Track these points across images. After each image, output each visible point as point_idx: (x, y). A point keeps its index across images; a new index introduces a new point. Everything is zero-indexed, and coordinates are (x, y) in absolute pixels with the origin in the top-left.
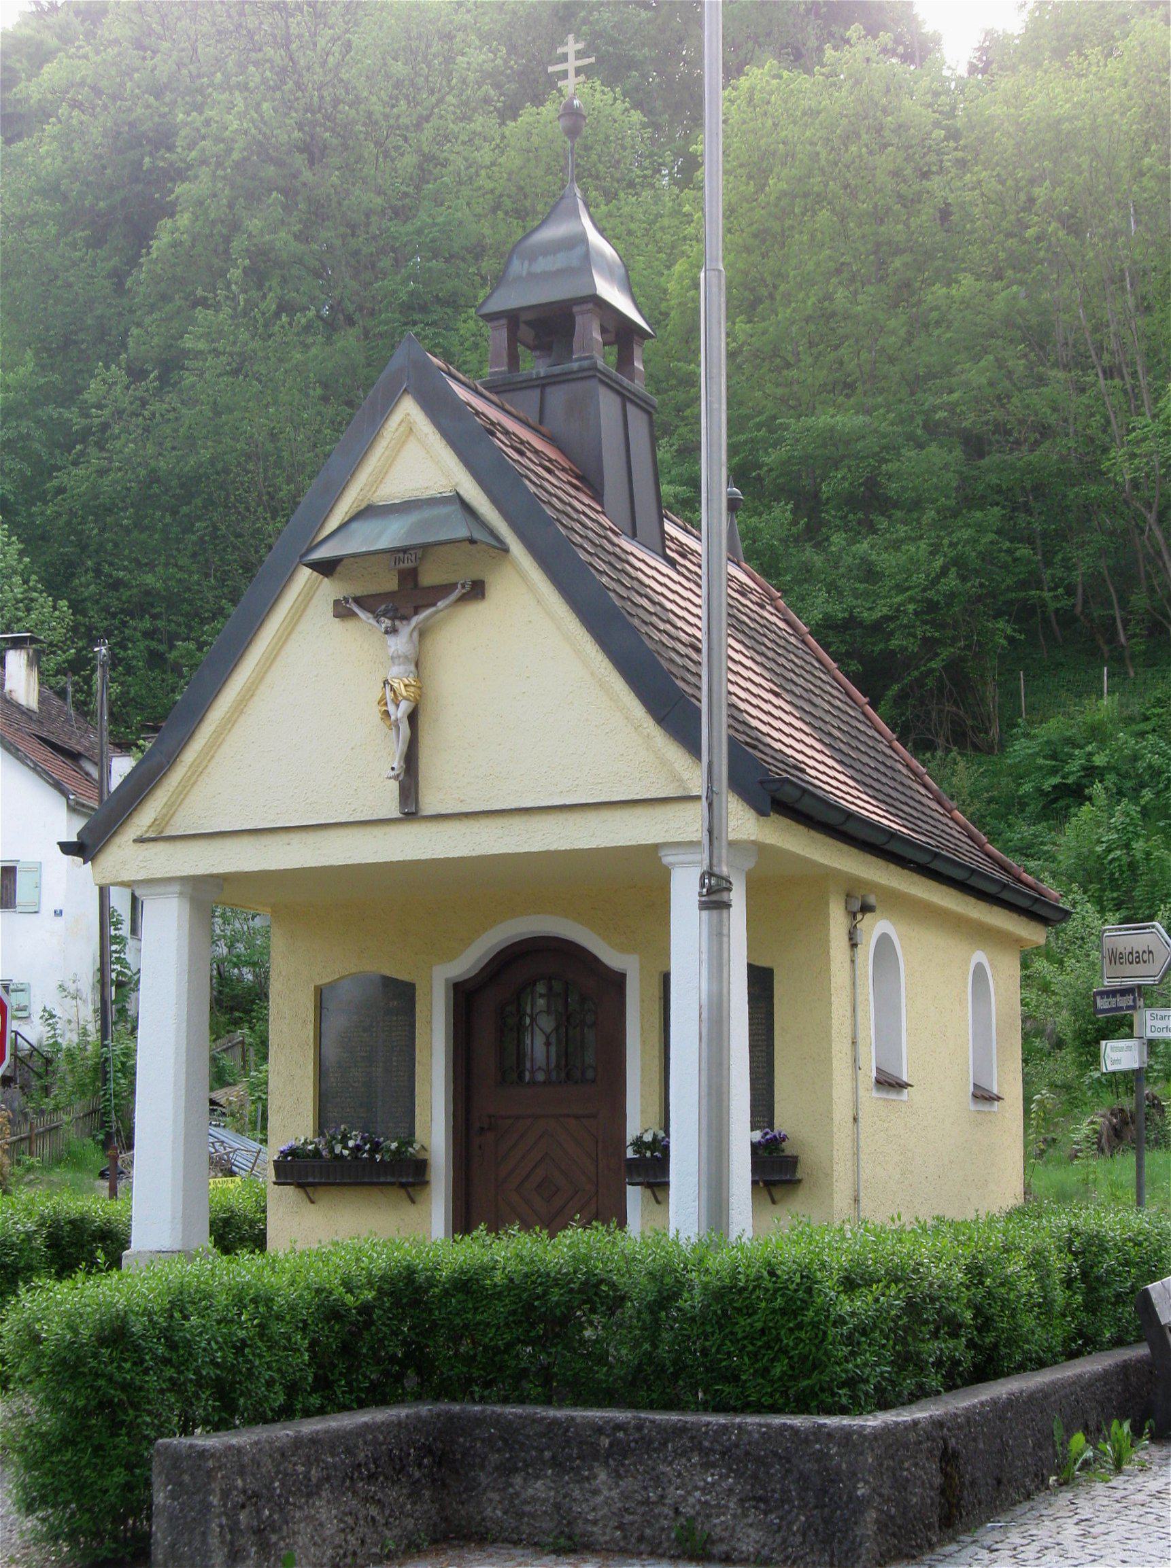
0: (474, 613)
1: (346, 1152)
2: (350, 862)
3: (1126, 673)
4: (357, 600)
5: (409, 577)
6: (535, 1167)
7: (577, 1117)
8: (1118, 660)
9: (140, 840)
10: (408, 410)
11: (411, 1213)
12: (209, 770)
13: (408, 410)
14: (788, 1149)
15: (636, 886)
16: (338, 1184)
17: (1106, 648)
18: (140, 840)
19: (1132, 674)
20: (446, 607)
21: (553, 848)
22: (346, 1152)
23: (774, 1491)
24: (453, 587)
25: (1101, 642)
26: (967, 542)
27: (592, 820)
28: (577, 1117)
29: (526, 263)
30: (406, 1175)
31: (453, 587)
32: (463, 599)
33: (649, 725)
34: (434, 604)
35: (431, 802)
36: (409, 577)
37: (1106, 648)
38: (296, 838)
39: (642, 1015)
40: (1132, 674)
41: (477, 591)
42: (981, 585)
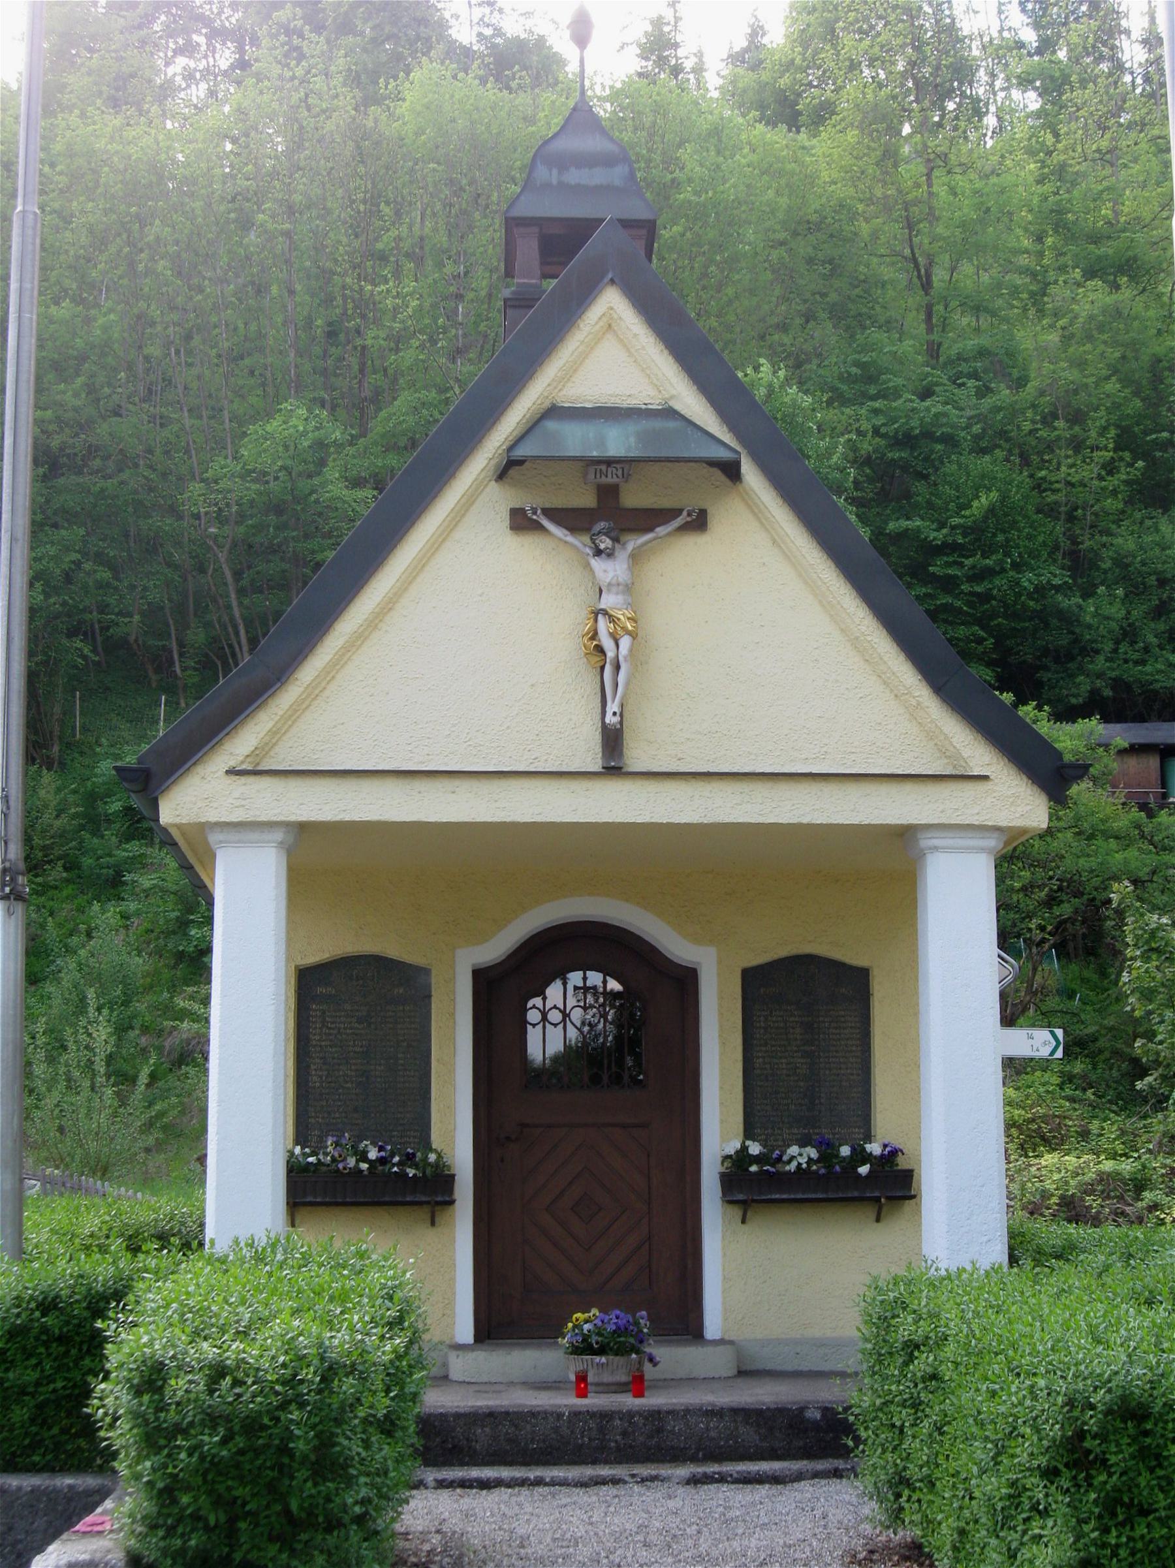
0: (692, 544)
1: (364, 1166)
2: (347, 818)
3: (178, 704)
4: (547, 512)
5: (608, 494)
6: (570, 1183)
7: (624, 1126)
8: (171, 690)
9: (232, 772)
10: (611, 303)
11: (429, 1237)
12: (327, 693)
13: (611, 303)
14: (902, 1163)
15: (885, 867)
16: (337, 1204)
17: (154, 678)
18: (232, 772)
19: (183, 705)
20: (669, 534)
21: (805, 821)
22: (364, 1166)
23: (473, 1527)
24: (677, 512)
25: (151, 673)
26: (52, 558)
27: (854, 791)
28: (624, 1126)
29: (555, 172)
30: (427, 1192)
31: (677, 512)
32: (686, 528)
33: (922, 693)
34: (651, 530)
35: (637, 756)
36: (608, 494)
37: (154, 678)
38: (464, 785)
39: (721, 1014)
40: (183, 705)
41: (699, 523)
42: (64, 604)
